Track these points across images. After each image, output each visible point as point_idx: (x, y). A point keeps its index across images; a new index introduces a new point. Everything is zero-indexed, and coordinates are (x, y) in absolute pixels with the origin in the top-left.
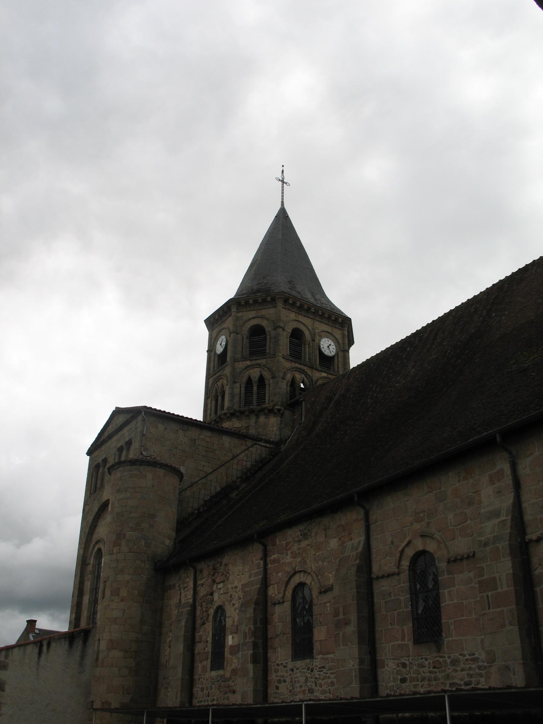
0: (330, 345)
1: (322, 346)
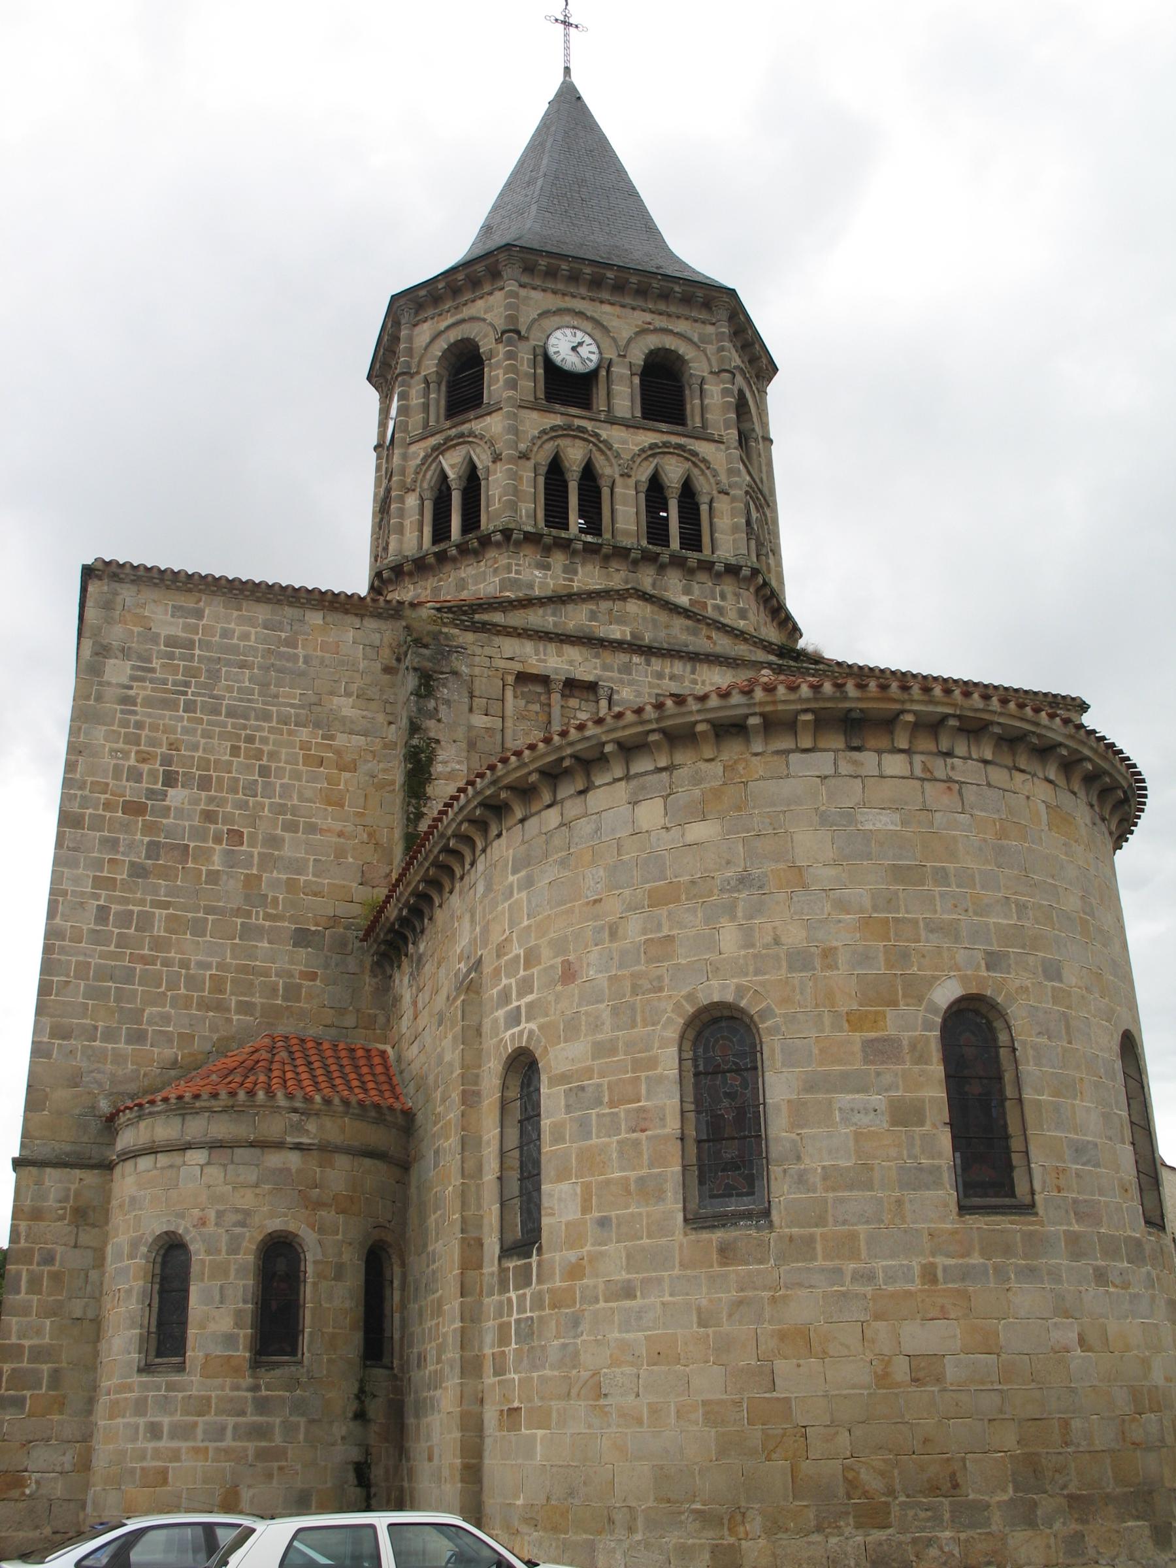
0: (580, 344)
1: (551, 350)
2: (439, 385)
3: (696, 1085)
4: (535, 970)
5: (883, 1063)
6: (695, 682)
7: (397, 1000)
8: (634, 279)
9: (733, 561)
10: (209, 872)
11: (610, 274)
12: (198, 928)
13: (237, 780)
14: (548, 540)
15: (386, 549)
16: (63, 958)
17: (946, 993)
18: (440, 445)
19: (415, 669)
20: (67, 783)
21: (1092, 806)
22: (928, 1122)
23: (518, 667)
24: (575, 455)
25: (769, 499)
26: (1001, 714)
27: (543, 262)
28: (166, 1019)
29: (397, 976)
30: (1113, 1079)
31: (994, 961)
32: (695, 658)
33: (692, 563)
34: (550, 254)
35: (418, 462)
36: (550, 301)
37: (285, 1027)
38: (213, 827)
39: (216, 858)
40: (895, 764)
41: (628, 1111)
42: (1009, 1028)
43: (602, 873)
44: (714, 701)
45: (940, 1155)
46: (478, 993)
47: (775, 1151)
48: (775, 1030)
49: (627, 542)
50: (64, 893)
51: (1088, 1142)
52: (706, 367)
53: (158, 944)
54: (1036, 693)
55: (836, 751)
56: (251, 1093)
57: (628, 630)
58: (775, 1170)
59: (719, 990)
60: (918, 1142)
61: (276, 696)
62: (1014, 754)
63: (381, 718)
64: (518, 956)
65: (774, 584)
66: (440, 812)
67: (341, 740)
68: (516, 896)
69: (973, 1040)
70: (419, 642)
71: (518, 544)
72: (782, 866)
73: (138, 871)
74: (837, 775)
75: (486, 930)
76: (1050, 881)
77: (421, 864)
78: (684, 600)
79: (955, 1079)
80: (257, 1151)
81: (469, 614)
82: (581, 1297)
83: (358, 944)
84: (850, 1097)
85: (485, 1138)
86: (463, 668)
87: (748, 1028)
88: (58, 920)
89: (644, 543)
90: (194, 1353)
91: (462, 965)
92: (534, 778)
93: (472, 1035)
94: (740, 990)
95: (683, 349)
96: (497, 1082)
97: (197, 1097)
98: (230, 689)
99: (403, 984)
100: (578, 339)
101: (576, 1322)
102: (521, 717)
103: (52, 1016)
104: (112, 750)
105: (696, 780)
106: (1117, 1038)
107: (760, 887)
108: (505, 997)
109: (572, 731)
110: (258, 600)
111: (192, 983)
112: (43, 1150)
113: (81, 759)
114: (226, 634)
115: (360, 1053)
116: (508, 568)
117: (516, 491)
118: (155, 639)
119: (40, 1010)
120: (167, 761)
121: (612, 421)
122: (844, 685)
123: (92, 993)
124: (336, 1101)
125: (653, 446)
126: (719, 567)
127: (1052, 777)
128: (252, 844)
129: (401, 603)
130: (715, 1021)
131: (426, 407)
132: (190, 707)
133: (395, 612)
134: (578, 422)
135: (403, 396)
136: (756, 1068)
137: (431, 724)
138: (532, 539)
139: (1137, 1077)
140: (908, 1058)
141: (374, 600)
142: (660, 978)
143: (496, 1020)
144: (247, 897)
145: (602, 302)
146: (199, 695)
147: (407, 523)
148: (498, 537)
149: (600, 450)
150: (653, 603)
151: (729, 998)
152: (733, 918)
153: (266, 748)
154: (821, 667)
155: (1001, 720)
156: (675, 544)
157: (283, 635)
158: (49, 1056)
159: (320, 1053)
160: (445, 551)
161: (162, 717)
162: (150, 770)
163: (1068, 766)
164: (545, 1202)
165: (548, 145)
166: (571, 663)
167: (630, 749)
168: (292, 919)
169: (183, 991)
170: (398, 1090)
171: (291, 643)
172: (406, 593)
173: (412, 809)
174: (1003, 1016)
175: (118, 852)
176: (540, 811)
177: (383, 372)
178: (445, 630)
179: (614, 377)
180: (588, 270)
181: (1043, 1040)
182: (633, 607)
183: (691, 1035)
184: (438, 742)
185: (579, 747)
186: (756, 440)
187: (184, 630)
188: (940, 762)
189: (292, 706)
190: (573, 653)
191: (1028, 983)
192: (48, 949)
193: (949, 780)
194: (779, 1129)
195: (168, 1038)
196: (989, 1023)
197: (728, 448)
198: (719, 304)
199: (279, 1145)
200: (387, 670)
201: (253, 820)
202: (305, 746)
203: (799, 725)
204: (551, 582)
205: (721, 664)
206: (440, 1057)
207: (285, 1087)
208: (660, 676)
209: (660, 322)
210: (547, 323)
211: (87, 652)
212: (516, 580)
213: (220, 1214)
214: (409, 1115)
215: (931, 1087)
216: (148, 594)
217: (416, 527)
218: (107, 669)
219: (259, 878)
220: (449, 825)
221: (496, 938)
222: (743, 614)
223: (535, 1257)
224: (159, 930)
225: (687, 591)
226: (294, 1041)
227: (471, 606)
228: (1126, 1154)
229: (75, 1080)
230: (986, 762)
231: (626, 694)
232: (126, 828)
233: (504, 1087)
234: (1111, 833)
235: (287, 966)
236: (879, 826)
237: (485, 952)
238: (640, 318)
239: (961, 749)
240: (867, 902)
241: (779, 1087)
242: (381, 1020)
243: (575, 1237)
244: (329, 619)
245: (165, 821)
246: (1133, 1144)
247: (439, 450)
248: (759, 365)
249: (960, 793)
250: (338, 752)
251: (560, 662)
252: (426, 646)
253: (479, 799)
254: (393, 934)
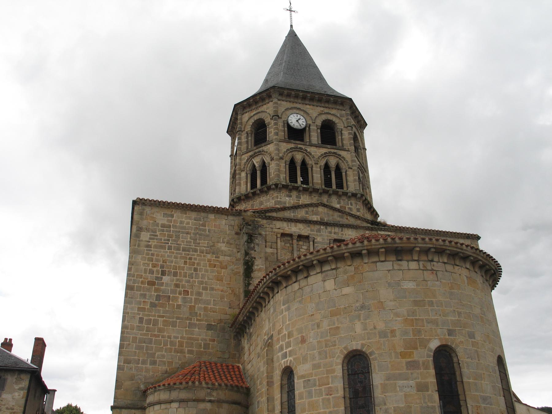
0: (299, 119)
1: (290, 122)
2: (252, 134)
3: (349, 379)
4: (292, 339)
5: (413, 369)
6: (343, 234)
7: (243, 348)
8: (317, 96)
9: (354, 192)
10: (177, 305)
11: (309, 95)
12: (174, 324)
13: (186, 273)
14: (290, 187)
15: (235, 191)
16: (128, 335)
17: (434, 344)
18: (252, 155)
19: (246, 233)
20: (128, 275)
21: (483, 276)
22: (430, 390)
23: (281, 231)
24: (299, 157)
25: (366, 169)
26: (449, 246)
27: (286, 92)
28: (163, 356)
29: (243, 340)
30: (495, 373)
31: (450, 332)
32: (342, 226)
33: (340, 193)
34: (288, 89)
35: (245, 161)
36: (289, 105)
37: (204, 358)
38: (178, 289)
39: (180, 300)
40: (413, 265)
41: (325, 388)
42: (457, 356)
43: (314, 305)
44: (350, 245)
45: (435, 402)
46: (272, 347)
47: (377, 401)
48: (375, 359)
49: (318, 187)
50: (128, 313)
51: (488, 396)
52: (342, 125)
53: (160, 330)
54: (461, 234)
55: (393, 261)
56: (193, 382)
57: (319, 217)
58: (377, 408)
59: (355, 345)
60: (427, 397)
61: (199, 244)
62: (454, 260)
63: (235, 250)
64: (285, 334)
65: (369, 199)
66: (257, 284)
67: (221, 258)
68: (284, 313)
69: (445, 362)
70: (247, 224)
71: (280, 189)
72: (376, 301)
73: (153, 305)
74: (393, 269)
75: (274, 325)
76: (469, 303)
77: (251, 302)
78: (338, 206)
79: (439, 374)
80: (196, 403)
81: (264, 213)
83: (229, 329)
84: (402, 382)
85: (276, 398)
87: (366, 358)
88: (126, 322)
89: (323, 187)
91: (266, 337)
92: (289, 273)
93: (270, 362)
94: (363, 345)
95: (334, 119)
96: (279, 378)
97: (175, 384)
98: (183, 241)
99: (245, 343)
100: (298, 118)
102: (283, 248)
103: (124, 356)
104: (143, 264)
105: (345, 272)
106: (496, 358)
107: (369, 309)
108: (281, 348)
109: (302, 257)
110: (192, 211)
111: (172, 344)
112: (121, 403)
113: (133, 267)
114: (181, 222)
115: (230, 367)
116: (277, 197)
117: (279, 170)
118: (157, 225)
119: (120, 354)
120: (162, 267)
121: (311, 145)
122: (395, 238)
123: (141, 348)
124: (223, 385)
125: (325, 153)
126: (350, 194)
127: (468, 267)
128: (192, 295)
129: (241, 210)
130: (354, 356)
131: (247, 142)
132: (170, 248)
133: (239, 213)
134: (299, 146)
135: (239, 139)
136: (369, 372)
137: (252, 252)
138: (285, 187)
139: (504, 372)
140: (422, 368)
141: (232, 210)
142: (335, 341)
143: (278, 356)
144: (190, 313)
145: (306, 104)
146: (173, 244)
147: (242, 182)
148: (274, 186)
149: (307, 155)
150: (327, 208)
151: (359, 348)
152: (359, 320)
153: (196, 262)
154: (386, 227)
155: (450, 248)
156: (334, 187)
157: (201, 222)
158: (123, 370)
159: (217, 367)
160: (255, 192)
161: (161, 252)
162: (157, 270)
163: (474, 263)
165: (286, 51)
166: (300, 229)
167: (322, 262)
168: (206, 321)
169: (169, 346)
170: (244, 380)
171: (204, 225)
172: (241, 207)
173: (246, 282)
174: (455, 352)
175: (146, 298)
176: (291, 284)
177: (232, 130)
178: (256, 219)
179: (311, 130)
180: (301, 94)
181: (469, 360)
182: (320, 209)
183: (346, 361)
184: (255, 258)
185: (305, 262)
186: (361, 149)
187: (167, 221)
188: (429, 264)
189: (204, 247)
190: (300, 226)
191: (463, 340)
192: (122, 333)
193: (432, 270)
194: (378, 394)
195: (164, 363)
196: (450, 354)
197: (351, 153)
198: (346, 103)
199: (203, 401)
200: (237, 234)
201: (192, 287)
202: (209, 261)
203: (380, 254)
204: (292, 202)
205: (351, 228)
206: (259, 371)
207: (205, 380)
208: (330, 233)
209: (326, 110)
210: (288, 112)
211: (134, 230)
212: (280, 201)
214: (248, 389)
215: (430, 377)
216: (155, 210)
217: (245, 183)
218: (141, 236)
219: (194, 306)
220: (260, 289)
221: (278, 328)
222: (358, 210)
224: (160, 325)
225: (339, 203)
226: (207, 363)
227: (265, 211)
228: (502, 400)
229: (132, 378)
230: (445, 263)
231: (319, 239)
232: (149, 290)
233: (282, 380)
234: (490, 285)
235: (204, 337)
236: (409, 287)
237: (274, 333)
238: (319, 109)
239: (436, 259)
240: (405, 313)
241: (378, 379)
242: (237, 355)
244: (217, 216)
245: (162, 288)
246: (504, 396)
247: (252, 157)
248: (361, 124)
249: (436, 274)
250: (221, 262)
251: (296, 229)
252: (250, 225)
253: (271, 280)
254: (240, 327)
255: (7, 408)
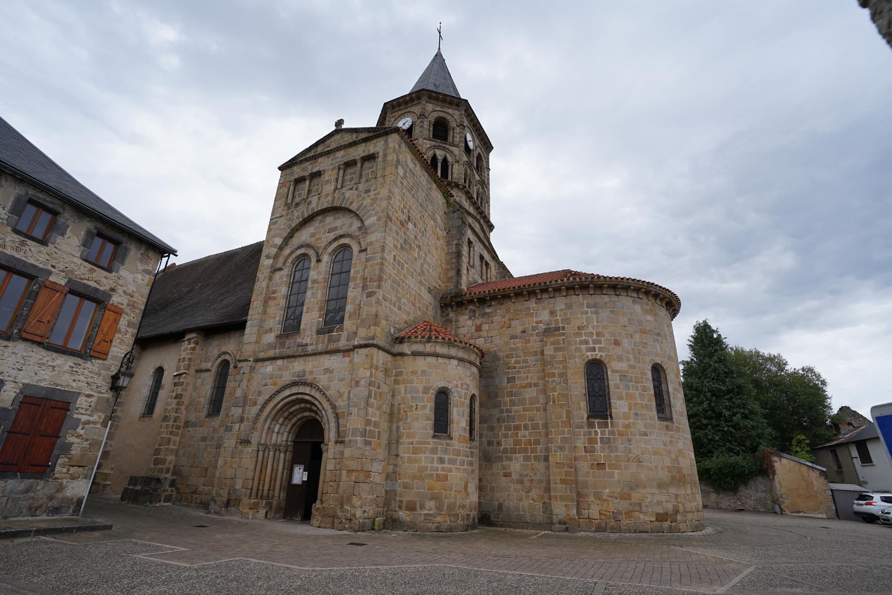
82: (481, 417)
86: (348, 194)
90: (154, 415)
95: (449, 118)
101: (630, 441)
164: (613, 405)
198: (464, 106)
213: (462, 384)
223: (609, 420)
239: (557, 294)
243: (626, 416)
255: (125, 292)
